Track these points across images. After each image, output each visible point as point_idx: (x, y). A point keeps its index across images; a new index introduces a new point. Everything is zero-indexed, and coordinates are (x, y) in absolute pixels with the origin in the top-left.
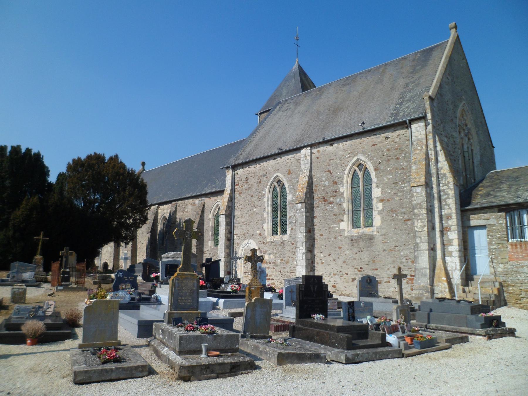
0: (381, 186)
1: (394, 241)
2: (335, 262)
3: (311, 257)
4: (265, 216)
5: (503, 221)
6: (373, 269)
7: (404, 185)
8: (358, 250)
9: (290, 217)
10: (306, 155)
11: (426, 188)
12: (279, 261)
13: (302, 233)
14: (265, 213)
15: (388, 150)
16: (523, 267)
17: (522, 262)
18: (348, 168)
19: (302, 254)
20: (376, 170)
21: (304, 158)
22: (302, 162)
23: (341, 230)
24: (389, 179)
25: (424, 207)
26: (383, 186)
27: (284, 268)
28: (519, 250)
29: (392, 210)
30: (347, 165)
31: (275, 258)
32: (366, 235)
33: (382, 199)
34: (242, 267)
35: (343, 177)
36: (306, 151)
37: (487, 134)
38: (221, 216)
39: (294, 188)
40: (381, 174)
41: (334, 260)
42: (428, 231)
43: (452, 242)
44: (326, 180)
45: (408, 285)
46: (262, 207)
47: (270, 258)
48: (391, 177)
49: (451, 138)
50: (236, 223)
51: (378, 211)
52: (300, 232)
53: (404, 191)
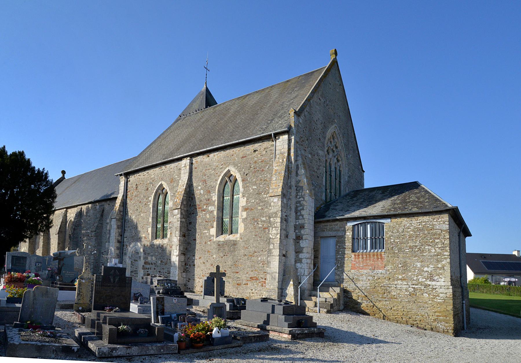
0: (246, 196)
1: (254, 247)
2: (204, 265)
3: (184, 260)
4: (150, 221)
5: (350, 232)
6: (235, 272)
7: (266, 196)
8: (224, 254)
9: (170, 222)
10: (186, 165)
11: (282, 198)
12: (160, 262)
13: (177, 237)
14: (150, 218)
15: (256, 162)
16: (362, 275)
17: (362, 270)
18: (221, 177)
19: (176, 256)
20: (243, 181)
21: (184, 168)
22: (182, 172)
23: (211, 235)
24: (253, 189)
25: (278, 216)
26: (248, 196)
27: (163, 269)
28: (360, 259)
29: (253, 219)
30: (220, 175)
31: (156, 259)
32: (231, 241)
33: (247, 208)
34: (130, 267)
35: (216, 186)
36: (186, 161)
37: (358, 159)
38: (113, 220)
39: (174, 196)
40: (248, 185)
41: (204, 263)
42: (280, 239)
43: (303, 250)
44: (201, 189)
45: (262, 288)
46: (148, 213)
47: (152, 259)
48: (256, 187)
49: (316, 155)
50: (126, 227)
51: (243, 219)
52: (175, 236)
53: (265, 201)
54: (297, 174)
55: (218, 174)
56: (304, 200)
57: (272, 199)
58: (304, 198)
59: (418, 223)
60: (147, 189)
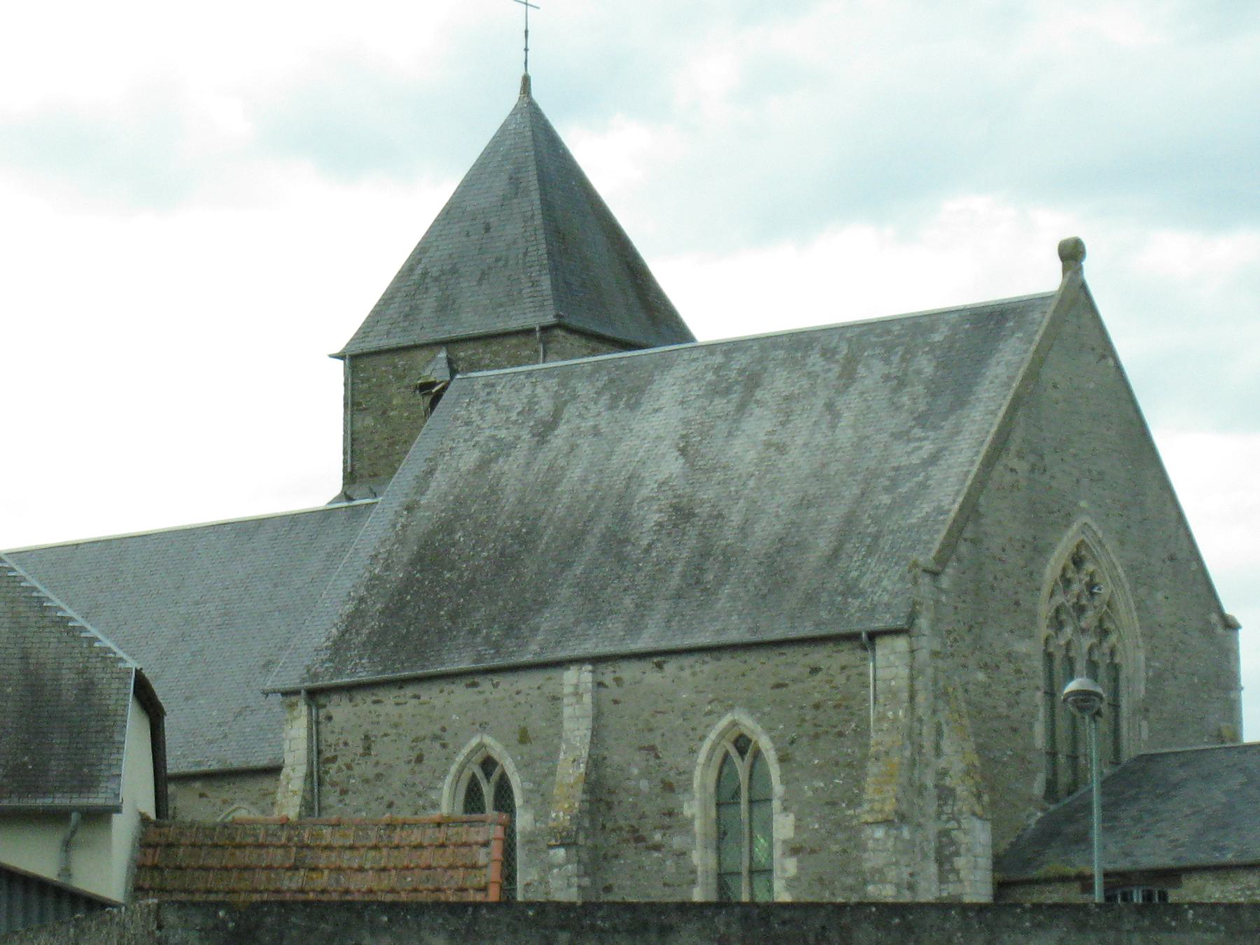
15: (817, 706)
24: (815, 790)
48: (822, 785)
54: (938, 751)
55: (699, 733)
56: (959, 828)
57: (868, 831)
58: (959, 822)
59: (1238, 890)
60: (419, 759)
